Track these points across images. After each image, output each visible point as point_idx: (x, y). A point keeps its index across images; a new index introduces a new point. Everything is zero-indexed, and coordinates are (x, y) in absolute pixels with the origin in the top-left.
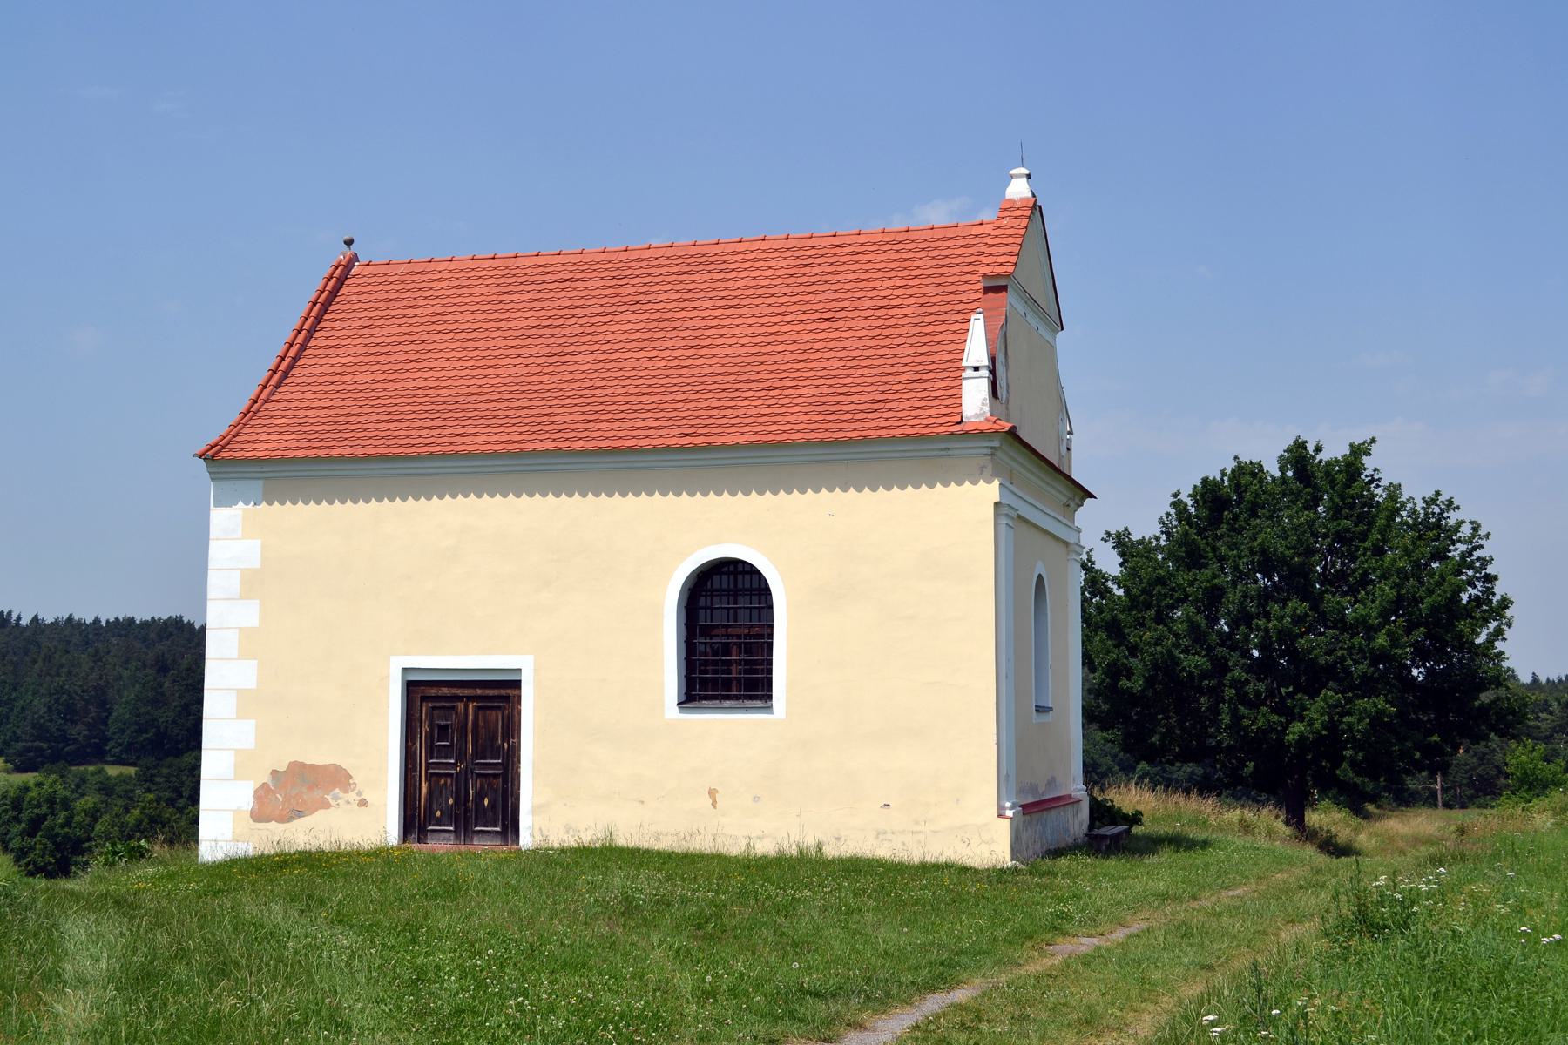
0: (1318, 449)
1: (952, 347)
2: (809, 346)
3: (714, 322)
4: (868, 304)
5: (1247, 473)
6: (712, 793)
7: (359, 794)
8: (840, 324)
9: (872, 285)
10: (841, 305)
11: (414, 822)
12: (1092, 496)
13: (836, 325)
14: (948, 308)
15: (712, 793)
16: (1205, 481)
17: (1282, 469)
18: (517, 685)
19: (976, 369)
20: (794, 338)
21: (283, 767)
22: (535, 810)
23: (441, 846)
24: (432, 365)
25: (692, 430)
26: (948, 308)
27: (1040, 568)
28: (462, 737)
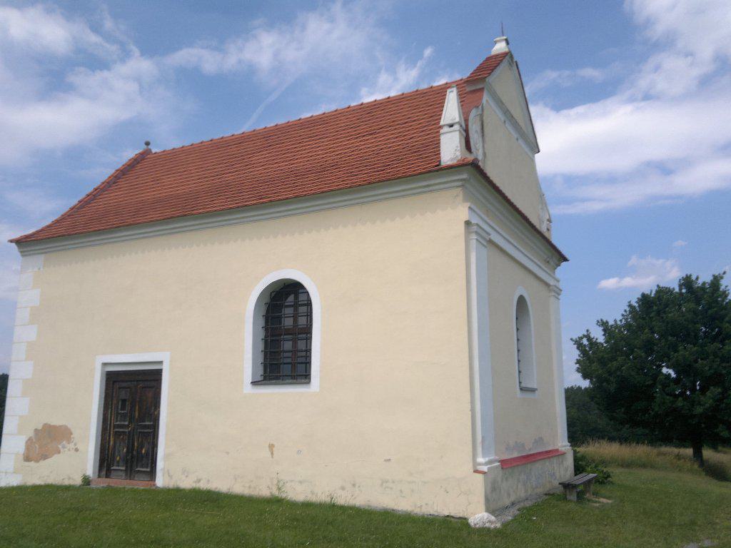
0: (697, 278)
5: (662, 292)
6: (271, 447)
7: (75, 445)
11: (106, 462)
12: (565, 259)
15: (271, 447)
16: (643, 295)
17: (680, 289)
18: (158, 373)
19: (451, 126)
21: (40, 427)
22: (167, 457)
23: (118, 481)
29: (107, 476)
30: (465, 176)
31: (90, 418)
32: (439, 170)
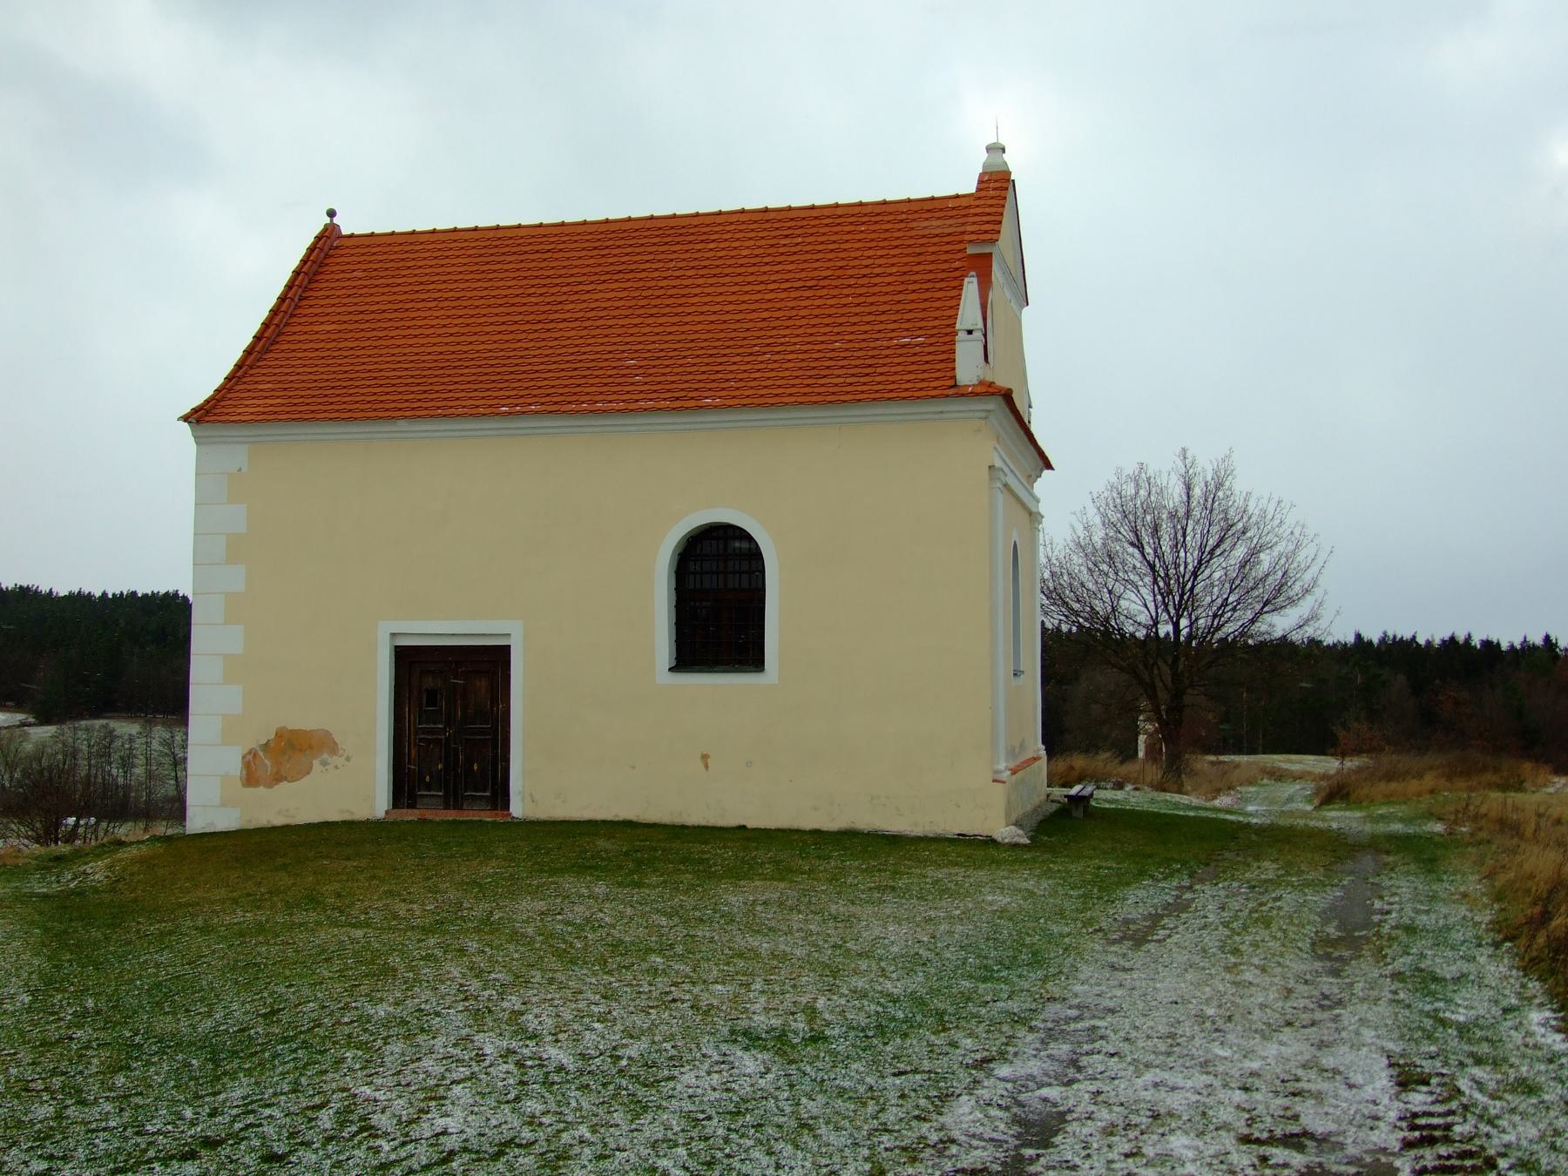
1: (949, 304)
2: (794, 313)
3: (697, 291)
4: (850, 272)
6: (705, 757)
8: (825, 292)
9: (853, 254)
10: (824, 274)
11: (404, 788)
12: (1049, 466)
13: (820, 293)
14: (930, 276)
15: (705, 757)
18: (505, 651)
19: (970, 332)
20: (778, 305)
24: (417, 332)
25: (682, 394)
26: (930, 276)
27: (1015, 537)
28: (452, 705)
29: (412, 806)
30: (991, 406)
31: (1087, 751)
32: (953, 390)
